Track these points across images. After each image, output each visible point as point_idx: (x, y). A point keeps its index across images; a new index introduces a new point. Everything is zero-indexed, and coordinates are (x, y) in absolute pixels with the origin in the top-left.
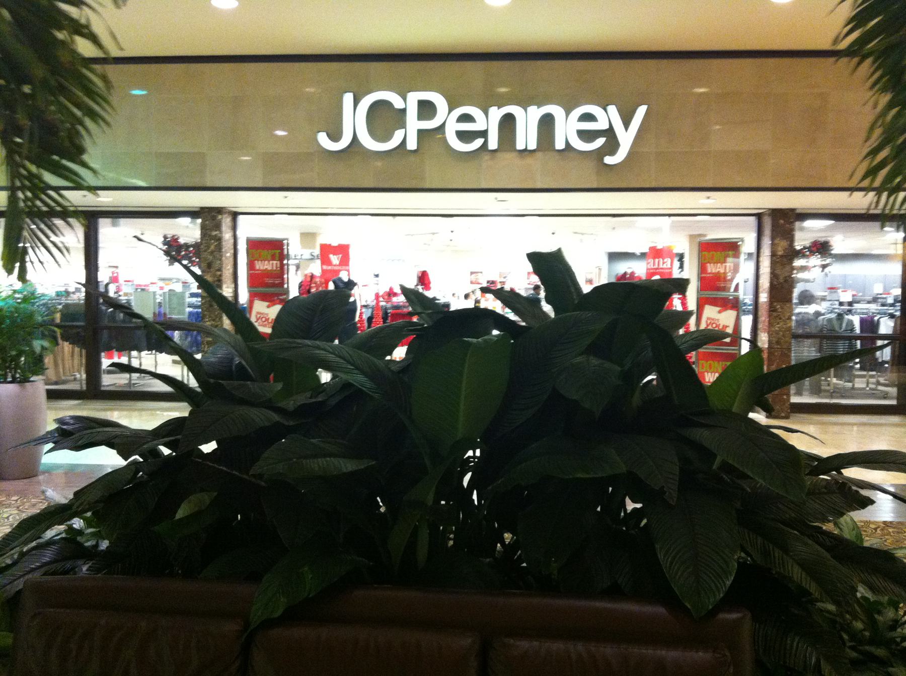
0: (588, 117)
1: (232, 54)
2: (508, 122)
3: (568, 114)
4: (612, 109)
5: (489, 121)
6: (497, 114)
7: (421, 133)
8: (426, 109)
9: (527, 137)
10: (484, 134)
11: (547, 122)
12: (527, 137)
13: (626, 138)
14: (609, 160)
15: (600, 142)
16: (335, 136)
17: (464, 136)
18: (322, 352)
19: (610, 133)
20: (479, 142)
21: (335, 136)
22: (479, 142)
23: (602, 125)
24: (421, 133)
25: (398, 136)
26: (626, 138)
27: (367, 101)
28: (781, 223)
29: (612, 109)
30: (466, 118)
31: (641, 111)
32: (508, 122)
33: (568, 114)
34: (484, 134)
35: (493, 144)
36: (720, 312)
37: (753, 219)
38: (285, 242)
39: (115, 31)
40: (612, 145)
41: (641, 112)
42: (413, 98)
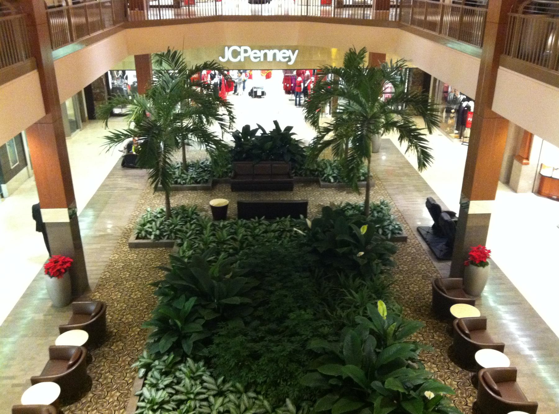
0: (284, 53)
1: (39, 85)
2: (265, 55)
3: (228, 59)
4: (290, 51)
5: (261, 54)
6: (263, 52)
7: (245, 57)
8: (246, 51)
9: (270, 58)
10: (260, 57)
12: (270, 58)
14: (289, 63)
15: (287, 59)
16: (223, 57)
17: (255, 58)
19: (289, 57)
20: (259, 59)
24: (245, 57)
25: (239, 58)
26: (293, 58)
27: (232, 48)
29: (290, 51)
32: (265, 55)
33: (228, 59)
35: (262, 59)
38: (235, 85)
41: (297, 52)
42: (243, 48)
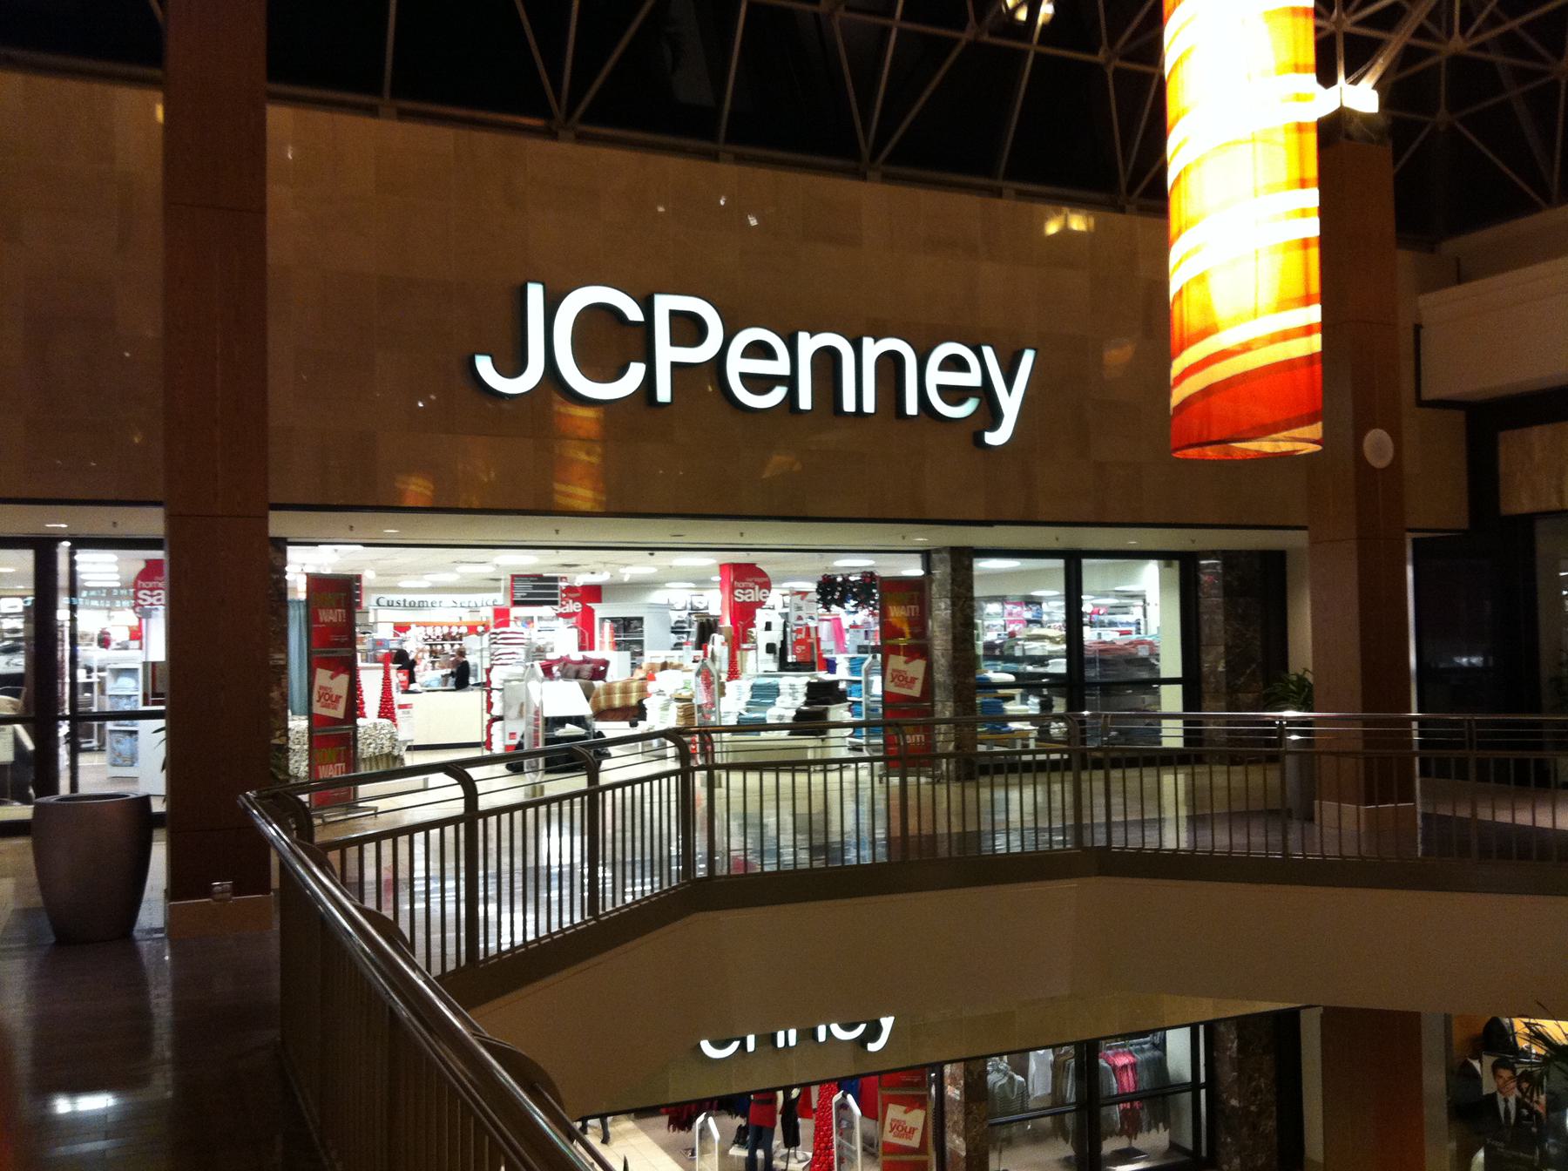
2: (827, 361)
11: (891, 366)
12: (859, 391)
13: (1010, 404)
17: (758, 384)
18: (444, 1050)
20: (778, 394)
21: (514, 364)
22: (778, 394)
23: (973, 379)
25: (637, 371)
26: (1010, 404)
28: (962, 558)
30: (760, 350)
31: (1028, 358)
34: (791, 381)
36: (332, 677)
37: (1059, 563)
39: (1182, 182)
40: (991, 413)
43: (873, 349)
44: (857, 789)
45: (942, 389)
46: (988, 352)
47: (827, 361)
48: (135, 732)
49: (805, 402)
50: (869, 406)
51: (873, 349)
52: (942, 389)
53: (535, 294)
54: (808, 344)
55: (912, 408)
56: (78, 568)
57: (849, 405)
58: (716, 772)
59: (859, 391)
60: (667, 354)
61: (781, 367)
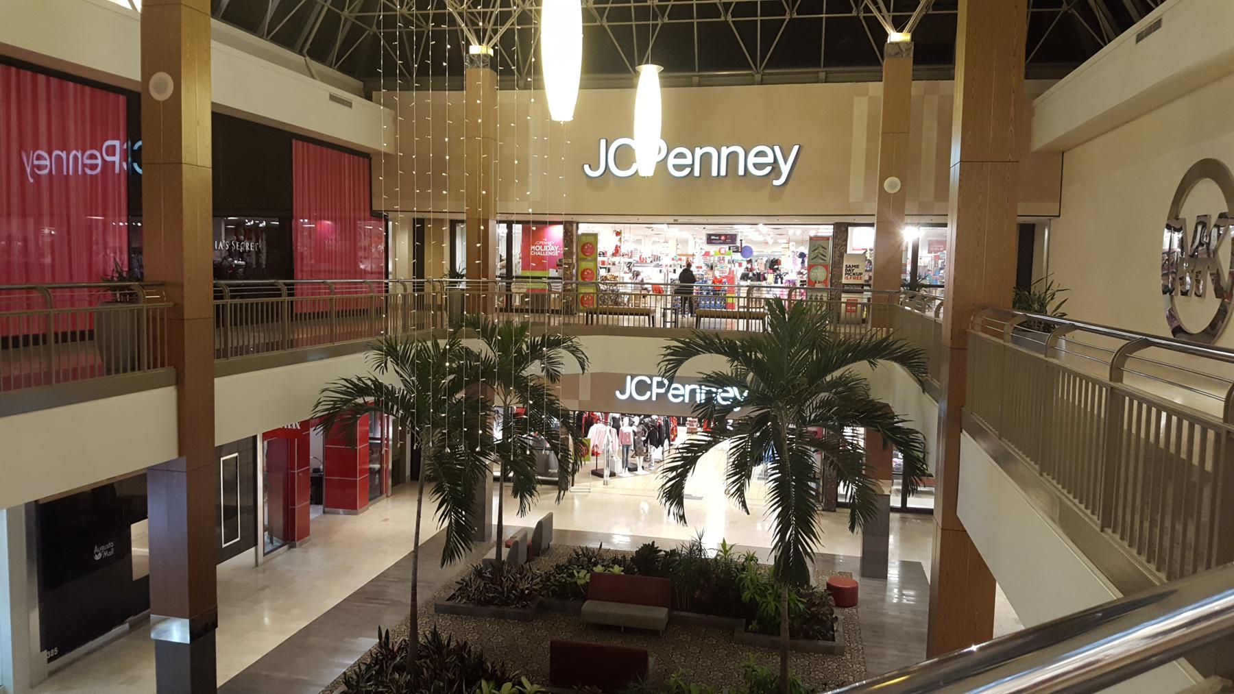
2: (706, 158)
11: (733, 157)
12: (718, 167)
17: (679, 168)
20: (681, 399)
21: (623, 393)
26: (785, 169)
34: (692, 166)
43: (725, 151)
44: (27, 270)
45: (755, 165)
46: (777, 149)
47: (706, 158)
48: (216, 298)
49: (697, 173)
50: (723, 173)
51: (725, 151)
52: (755, 165)
53: (603, 142)
54: (699, 152)
55: (741, 172)
56: (111, 95)
57: (714, 173)
58: (899, 505)
59: (718, 167)
60: (655, 390)
61: (688, 161)
